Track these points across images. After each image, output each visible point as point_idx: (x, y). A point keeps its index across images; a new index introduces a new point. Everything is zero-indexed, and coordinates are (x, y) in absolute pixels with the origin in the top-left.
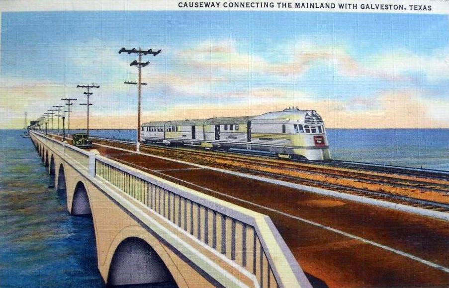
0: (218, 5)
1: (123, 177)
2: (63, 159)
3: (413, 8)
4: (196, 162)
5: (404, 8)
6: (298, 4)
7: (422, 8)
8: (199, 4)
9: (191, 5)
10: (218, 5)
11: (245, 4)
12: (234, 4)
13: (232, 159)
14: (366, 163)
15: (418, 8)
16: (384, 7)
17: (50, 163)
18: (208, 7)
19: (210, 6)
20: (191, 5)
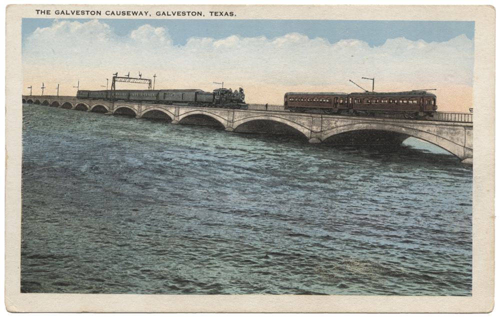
0: (146, 14)
1: (425, 136)
2: (235, 149)
3: (213, 14)
4: (352, 132)
5: (202, 15)
6: (135, 14)
7: (224, 14)
8: (126, 13)
9: (119, 14)
10: (146, 14)
11: (46, 12)
12: (96, 12)
13: (369, 122)
14: (421, 123)
15: (219, 14)
16: (80, 13)
17: (360, 125)
18: (136, 14)
19: (138, 14)
20: (119, 14)
